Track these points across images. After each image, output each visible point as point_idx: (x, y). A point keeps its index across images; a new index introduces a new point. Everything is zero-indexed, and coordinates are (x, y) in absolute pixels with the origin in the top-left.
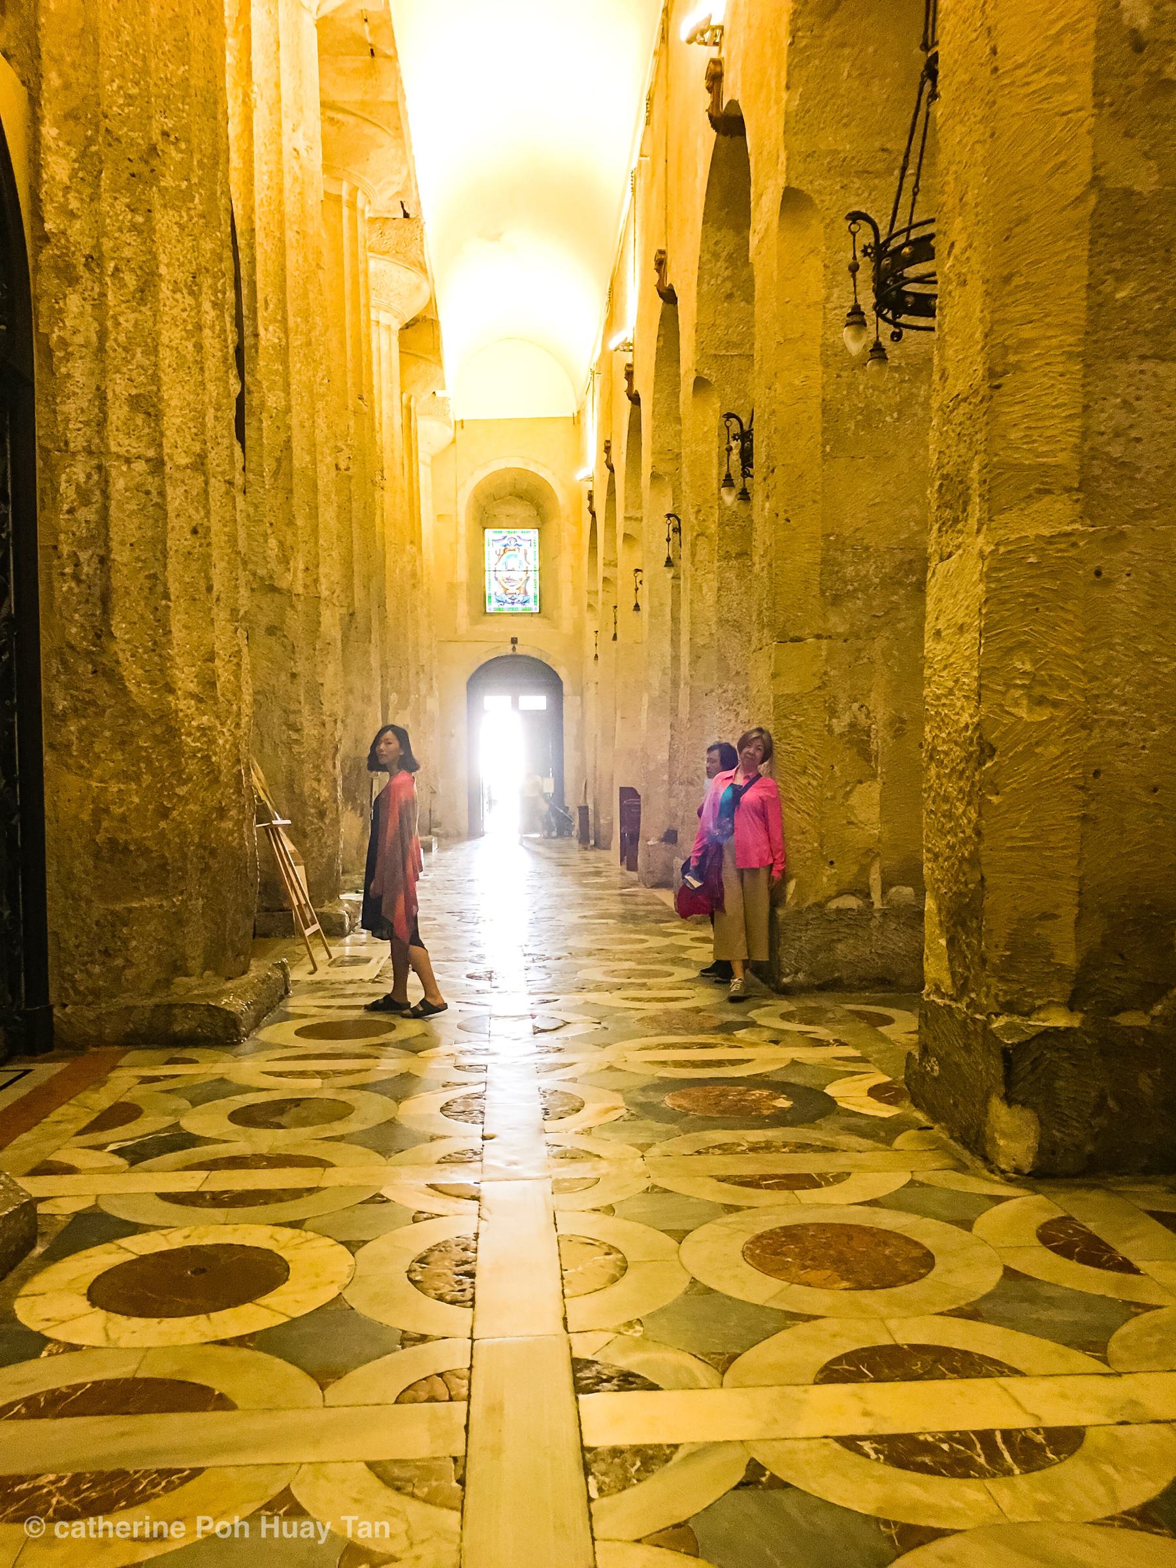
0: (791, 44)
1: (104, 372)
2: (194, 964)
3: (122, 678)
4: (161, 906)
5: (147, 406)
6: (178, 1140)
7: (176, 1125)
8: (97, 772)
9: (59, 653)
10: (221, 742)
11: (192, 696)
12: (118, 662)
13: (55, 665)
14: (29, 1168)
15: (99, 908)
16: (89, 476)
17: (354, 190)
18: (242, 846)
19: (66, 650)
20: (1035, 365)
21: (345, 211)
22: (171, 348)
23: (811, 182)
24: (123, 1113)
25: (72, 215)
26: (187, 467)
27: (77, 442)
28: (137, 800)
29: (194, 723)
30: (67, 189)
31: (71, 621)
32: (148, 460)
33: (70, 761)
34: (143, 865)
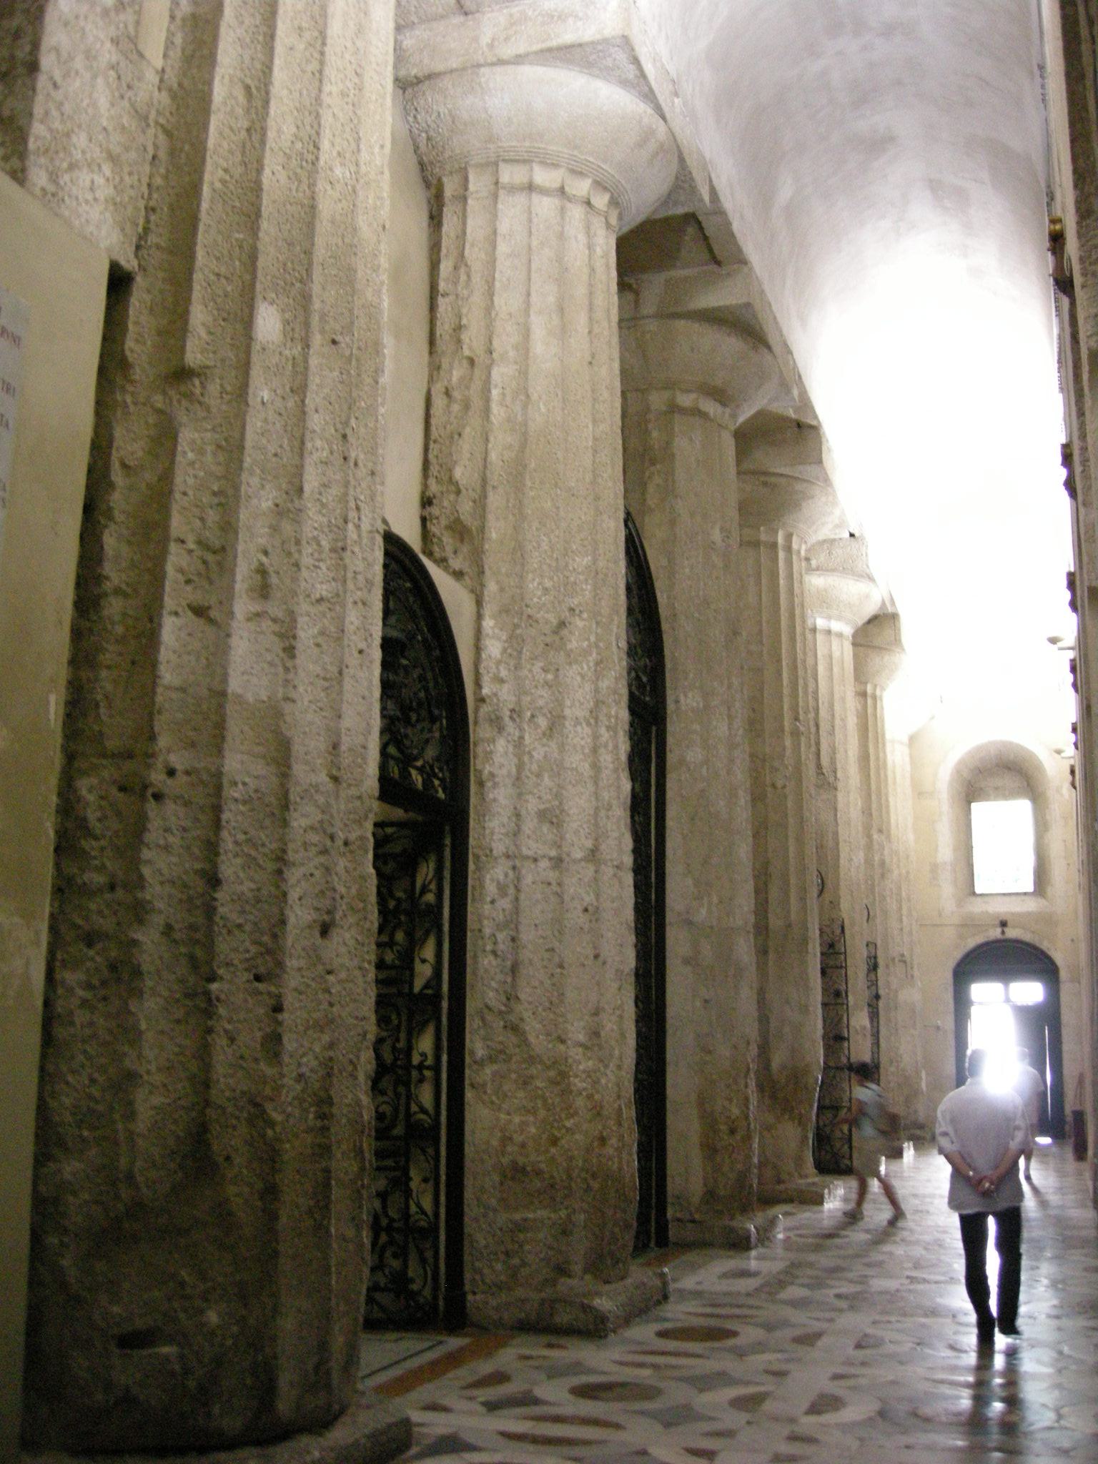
1: (520, 795)
2: (577, 1268)
3: (524, 1032)
5: (552, 817)
6: (527, 1400)
7: (531, 1391)
10: (603, 1081)
12: (522, 1019)
13: (478, 1022)
14: (422, 1404)
15: (502, 1218)
16: (506, 875)
17: (789, 537)
18: (620, 1169)
19: (486, 1011)
21: (781, 555)
22: (572, 769)
24: (500, 1378)
25: (502, 681)
27: (499, 848)
29: (581, 1067)
30: (499, 662)
31: (489, 987)
32: (551, 859)
33: (485, 1097)
34: (538, 1184)
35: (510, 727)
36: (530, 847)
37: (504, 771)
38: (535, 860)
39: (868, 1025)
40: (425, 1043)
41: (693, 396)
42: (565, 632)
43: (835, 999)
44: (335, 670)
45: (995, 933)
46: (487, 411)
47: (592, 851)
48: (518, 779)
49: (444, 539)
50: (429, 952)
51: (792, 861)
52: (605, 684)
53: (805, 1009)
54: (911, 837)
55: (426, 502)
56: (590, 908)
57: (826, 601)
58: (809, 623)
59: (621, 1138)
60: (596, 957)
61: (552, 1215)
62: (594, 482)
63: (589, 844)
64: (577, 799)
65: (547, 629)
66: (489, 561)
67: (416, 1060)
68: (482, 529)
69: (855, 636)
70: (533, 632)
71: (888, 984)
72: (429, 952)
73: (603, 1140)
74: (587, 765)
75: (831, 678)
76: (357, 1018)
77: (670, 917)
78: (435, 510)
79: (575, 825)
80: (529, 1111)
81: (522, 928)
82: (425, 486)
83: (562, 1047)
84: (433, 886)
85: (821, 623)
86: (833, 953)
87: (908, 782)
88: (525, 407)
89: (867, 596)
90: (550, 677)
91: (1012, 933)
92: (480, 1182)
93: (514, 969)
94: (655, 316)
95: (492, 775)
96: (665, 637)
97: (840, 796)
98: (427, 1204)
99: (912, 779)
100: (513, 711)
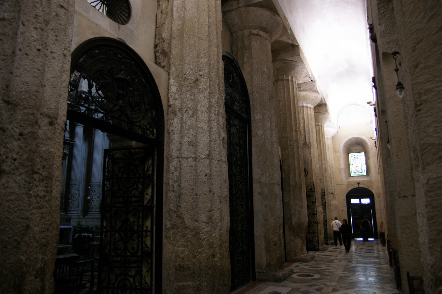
0: (379, 12)
1: (182, 136)
3: (183, 218)
4: (193, 285)
5: (193, 144)
8: (177, 245)
9: (168, 212)
10: (214, 235)
11: (205, 222)
12: (182, 214)
13: (167, 214)
16: (177, 164)
17: (292, 78)
19: (170, 211)
20: (434, 99)
21: (290, 83)
22: (201, 128)
23: (391, 49)
25: (176, 99)
26: (204, 158)
27: (175, 155)
28: (187, 253)
29: (205, 230)
30: (175, 93)
32: (193, 158)
35: (179, 114)
36: (185, 154)
37: (176, 129)
38: (187, 158)
39: (322, 210)
40: (148, 223)
41: (257, 30)
42: (198, 83)
43: (311, 205)
44: (10, 51)
45: (357, 186)
46: (172, 14)
47: (208, 155)
48: (181, 131)
49: (160, 57)
50: (149, 191)
51: (296, 166)
52: (214, 100)
53: (301, 207)
54: (333, 162)
55: (156, 46)
56: (208, 175)
57: (305, 99)
58: (300, 105)
59: (221, 254)
60: (210, 191)
61: (194, 284)
62: (209, 35)
63: (207, 153)
64: (203, 138)
65: (192, 82)
66: (172, 61)
67: (145, 229)
68: (170, 52)
69: (314, 108)
70: (187, 83)
71: (328, 199)
72: (149, 191)
73: (214, 256)
74: (206, 127)
75: (308, 119)
76: (22, 218)
77: (254, 181)
78: (157, 49)
79: (202, 146)
80: (185, 246)
81: (182, 182)
82: (155, 41)
83: (197, 223)
84: (151, 169)
85: (305, 105)
86: (310, 193)
87: (332, 148)
88: (184, 12)
89: (317, 97)
90: (193, 97)
91: (361, 186)
92: (168, 271)
93: (179, 196)
94: (243, 6)
95: (173, 130)
96: (250, 99)
97: (312, 150)
98: (148, 280)
99: (333, 147)
100: (179, 109)
